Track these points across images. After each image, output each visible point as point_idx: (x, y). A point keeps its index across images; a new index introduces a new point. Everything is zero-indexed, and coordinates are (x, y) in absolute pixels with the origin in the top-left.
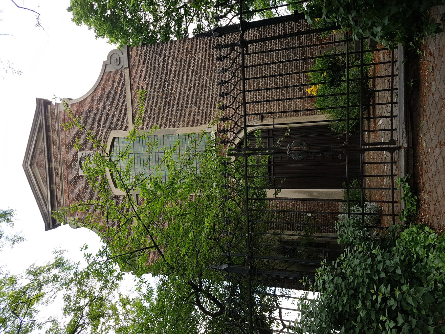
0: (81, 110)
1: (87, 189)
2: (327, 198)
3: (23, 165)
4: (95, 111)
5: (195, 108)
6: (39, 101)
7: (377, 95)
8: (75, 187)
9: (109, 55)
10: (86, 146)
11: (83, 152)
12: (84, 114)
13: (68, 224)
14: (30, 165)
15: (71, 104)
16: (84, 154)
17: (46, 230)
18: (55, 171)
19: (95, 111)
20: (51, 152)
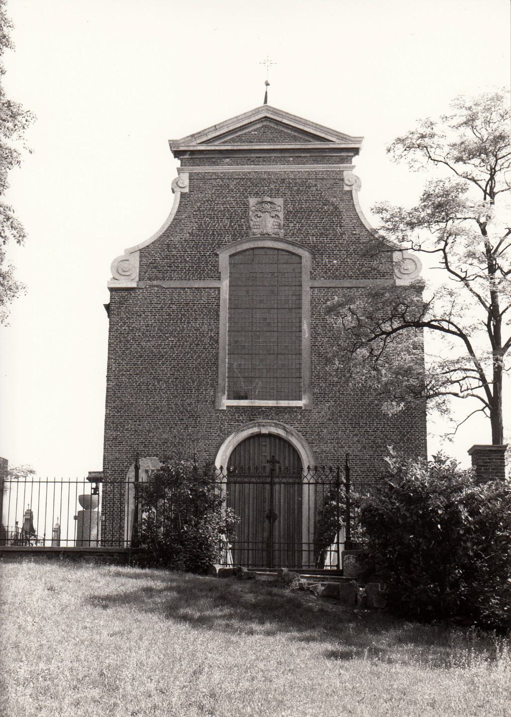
0: (342, 206)
1: (229, 211)
2: (126, 286)
3: (475, 446)
4: (339, 230)
5: (335, 379)
6: (359, 140)
7: (277, 489)
8: (232, 191)
9: (419, 260)
10: (291, 212)
11: (282, 207)
12: (336, 212)
13: (177, 176)
14: (266, 117)
15: (351, 191)
16: (279, 208)
17: (169, 141)
18: (257, 157)
19: (339, 230)
20: (285, 153)
